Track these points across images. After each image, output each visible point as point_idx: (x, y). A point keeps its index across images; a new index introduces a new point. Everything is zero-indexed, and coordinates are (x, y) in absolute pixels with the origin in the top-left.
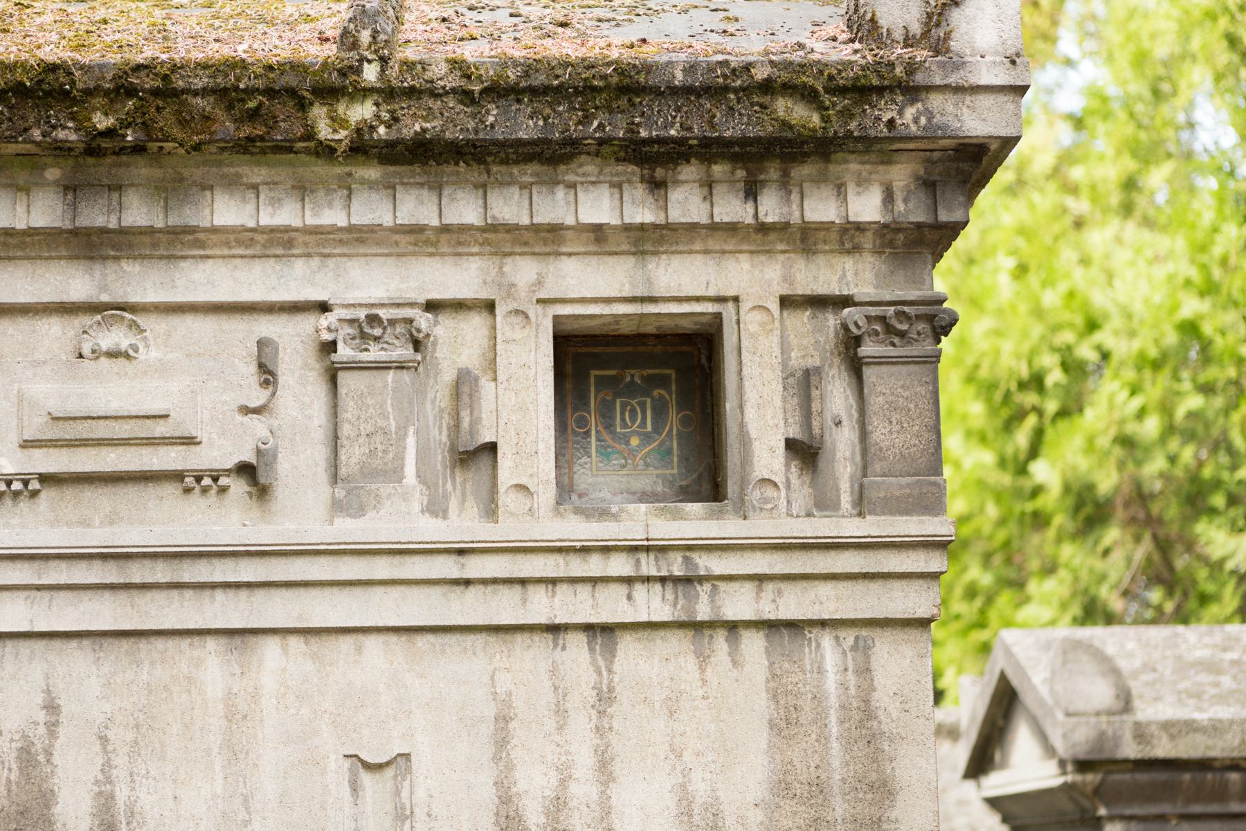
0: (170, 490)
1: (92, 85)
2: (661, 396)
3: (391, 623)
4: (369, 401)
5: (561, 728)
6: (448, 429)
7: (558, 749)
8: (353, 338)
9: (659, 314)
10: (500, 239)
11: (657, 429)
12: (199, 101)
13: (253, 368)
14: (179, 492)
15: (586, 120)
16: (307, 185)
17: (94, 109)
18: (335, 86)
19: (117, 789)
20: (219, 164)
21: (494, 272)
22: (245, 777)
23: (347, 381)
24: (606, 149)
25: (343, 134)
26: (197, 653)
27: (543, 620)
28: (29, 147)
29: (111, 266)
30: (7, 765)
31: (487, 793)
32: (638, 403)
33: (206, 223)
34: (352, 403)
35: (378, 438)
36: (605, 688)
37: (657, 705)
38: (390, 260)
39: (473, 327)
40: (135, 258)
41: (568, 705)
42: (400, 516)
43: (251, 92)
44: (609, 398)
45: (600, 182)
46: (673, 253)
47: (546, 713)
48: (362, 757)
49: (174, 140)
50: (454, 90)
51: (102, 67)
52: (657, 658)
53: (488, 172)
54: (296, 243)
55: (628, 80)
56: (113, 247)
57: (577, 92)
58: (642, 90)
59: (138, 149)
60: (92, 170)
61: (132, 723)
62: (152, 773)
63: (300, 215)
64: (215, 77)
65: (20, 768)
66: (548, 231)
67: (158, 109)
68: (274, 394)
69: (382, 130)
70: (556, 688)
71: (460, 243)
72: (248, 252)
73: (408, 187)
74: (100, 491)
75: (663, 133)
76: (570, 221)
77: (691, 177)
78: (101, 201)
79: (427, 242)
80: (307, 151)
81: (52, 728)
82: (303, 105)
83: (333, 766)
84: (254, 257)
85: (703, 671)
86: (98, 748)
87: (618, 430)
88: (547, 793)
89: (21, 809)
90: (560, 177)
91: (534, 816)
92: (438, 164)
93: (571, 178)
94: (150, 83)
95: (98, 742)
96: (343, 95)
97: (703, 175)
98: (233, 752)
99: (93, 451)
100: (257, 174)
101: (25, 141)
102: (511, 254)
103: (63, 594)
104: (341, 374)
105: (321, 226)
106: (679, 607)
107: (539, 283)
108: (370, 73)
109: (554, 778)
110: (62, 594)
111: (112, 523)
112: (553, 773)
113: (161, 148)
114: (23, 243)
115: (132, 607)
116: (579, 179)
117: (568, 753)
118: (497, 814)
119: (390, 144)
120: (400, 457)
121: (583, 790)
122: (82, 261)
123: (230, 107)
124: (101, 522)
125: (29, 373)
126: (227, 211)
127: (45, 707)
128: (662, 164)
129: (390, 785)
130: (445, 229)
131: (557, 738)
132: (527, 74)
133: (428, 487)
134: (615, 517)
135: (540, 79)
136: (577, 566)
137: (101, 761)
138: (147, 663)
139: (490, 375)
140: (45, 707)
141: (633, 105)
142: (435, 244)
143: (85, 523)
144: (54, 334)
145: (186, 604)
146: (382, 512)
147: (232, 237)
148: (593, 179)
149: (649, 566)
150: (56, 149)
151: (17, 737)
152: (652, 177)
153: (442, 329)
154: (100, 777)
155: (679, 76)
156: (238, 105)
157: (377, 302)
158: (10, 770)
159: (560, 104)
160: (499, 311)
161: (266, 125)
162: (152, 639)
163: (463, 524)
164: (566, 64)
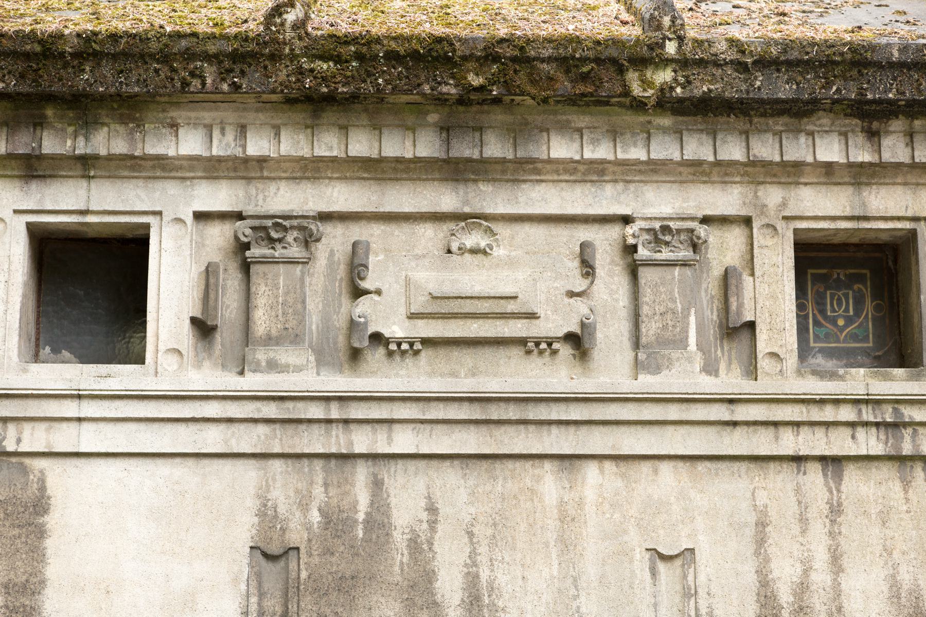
0: (516, 352)
1: (468, 53)
2: (860, 290)
3: (680, 453)
4: (662, 289)
5: (804, 532)
6: (718, 310)
7: (802, 548)
8: (650, 243)
9: (871, 229)
10: (757, 172)
11: (857, 313)
12: (545, 66)
13: (576, 263)
14: (522, 353)
15: (828, 85)
16: (618, 129)
17: (468, 71)
18: (645, 57)
19: (481, 570)
20: (555, 113)
21: (751, 196)
22: (574, 564)
23: (646, 275)
24: (837, 107)
25: (650, 92)
26: (537, 471)
27: (791, 453)
28: (417, 98)
29: (471, 187)
30: (400, 551)
31: (751, 579)
32: (843, 294)
33: (544, 156)
34: (649, 290)
35: (669, 316)
36: (835, 504)
37: (874, 516)
38: (675, 186)
39: (735, 237)
40: (489, 181)
41: (809, 515)
42: (684, 375)
43: (584, 60)
44: (822, 290)
45: (831, 131)
46: (881, 184)
47: (793, 521)
48: (659, 550)
49: (528, 95)
50: (731, 61)
51: (474, 39)
52: (873, 482)
53: (751, 122)
54: (607, 172)
55: (859, 57)
56: (473, 173)
57: (822, 65)
58: (867, 64)
59: (497, 101)
60: (462, 116)
61: (491, 522)
62: (507, 559)
63: (613, 151)
64: (558, 49)
65: (410, 554)
66: (793, 167)
67: (515, 71)
68: (592, 282)
69: (679, 90)
70: (800, 503)
71: (726, 174)
72: (572, 178)
73: (692, 132)
74: (465, 351)
75: (883, 96)
76: (810, 159)
77: (898, 129)
78: (467, 138)
79: (703, 173)
80: (621, 105)
81: (433, 524)
82: (621, 71)
83: (638, 556)
84: (575, 181)
85: (906, 492)
86: (466, 540)
87: (829, 314)
88: (795, 579)
89: (411, 583)
90: (803, 127)
91: (785, 597)
92: (715, 116)
93: (810, 127)
94: (510, 52)
95: (467, 536)
96: (650, 64)
97: (907, 127)
98: (566, 545)
99: (461, 322)
100: (582, 121)
101: (418, 94)
102: (763, 183)
103: (440, 427)
104: (641, 269)
105: (629, 160)
106: (889, 445)
107: (784, 205)
108: (671, 48)
109: (799, 569)
110: (439, 426)
111: (474, 375)
112: (798, 565)
113: (513, 100)
114: (408, 168)
115: (491, 436)
116: (817, 129)
117: (809, 550)
118: (758, 594)
119: (681, 100)
120: (685, 331)
121: (821, 577)
122: (450, 183)
123: (567, 71)
124: (466, 375)
125: (413, 264)
126: (561, 148)
127: (427, 509)
128: (878, 119)
129: (679, 571)
130: (718, 163)
131: (801, 539)
132: (785, 51)
133: (704, 354)
134: (842, 378)
135: (794, 55)
136: (816, 414)
137: (469, 550)
138: (501, 478)
139: (748, 271)
140: (427, 509)
141: (862, 75)
142: (708, 175)
143: (454, 374)
144: (429, 236)
145: (530, 435)
146: (673, 371)
147: (561, 167)
148: (827, 129)
149: (868, 415)
150: (436, 99)
151: (407, 531)
152: (870, 128)
153: (711, 235)
154: (468, 561)
155: (896, 54)
156: (574, 70)
157: (668, 216)
158: (402, 554)
159: (808, 73)
160: (756, 225)
161: (594, 85)
162: (504, 461)
163: (729, 381)
164: (813, 44)
